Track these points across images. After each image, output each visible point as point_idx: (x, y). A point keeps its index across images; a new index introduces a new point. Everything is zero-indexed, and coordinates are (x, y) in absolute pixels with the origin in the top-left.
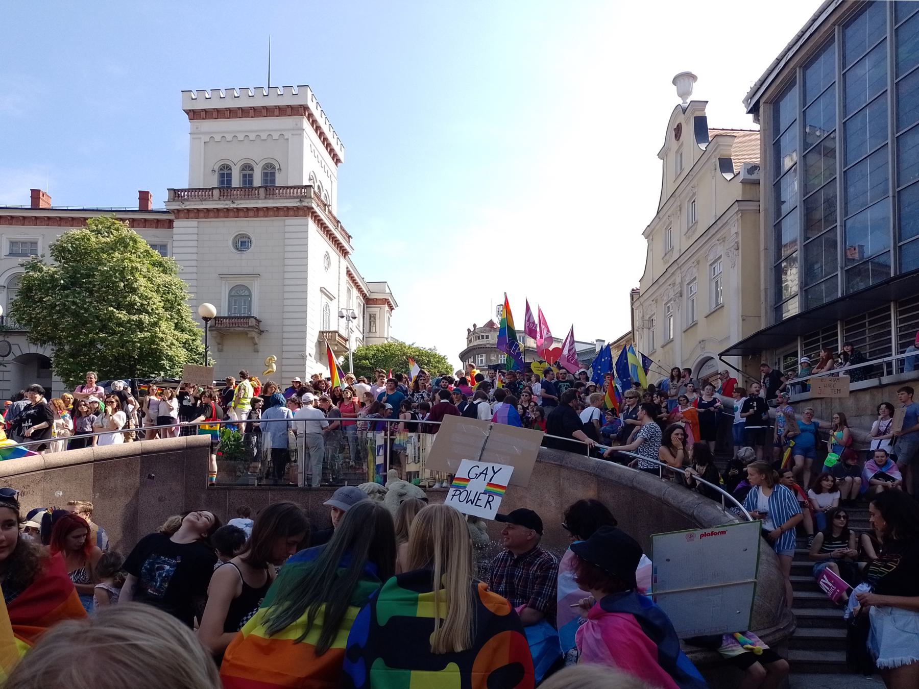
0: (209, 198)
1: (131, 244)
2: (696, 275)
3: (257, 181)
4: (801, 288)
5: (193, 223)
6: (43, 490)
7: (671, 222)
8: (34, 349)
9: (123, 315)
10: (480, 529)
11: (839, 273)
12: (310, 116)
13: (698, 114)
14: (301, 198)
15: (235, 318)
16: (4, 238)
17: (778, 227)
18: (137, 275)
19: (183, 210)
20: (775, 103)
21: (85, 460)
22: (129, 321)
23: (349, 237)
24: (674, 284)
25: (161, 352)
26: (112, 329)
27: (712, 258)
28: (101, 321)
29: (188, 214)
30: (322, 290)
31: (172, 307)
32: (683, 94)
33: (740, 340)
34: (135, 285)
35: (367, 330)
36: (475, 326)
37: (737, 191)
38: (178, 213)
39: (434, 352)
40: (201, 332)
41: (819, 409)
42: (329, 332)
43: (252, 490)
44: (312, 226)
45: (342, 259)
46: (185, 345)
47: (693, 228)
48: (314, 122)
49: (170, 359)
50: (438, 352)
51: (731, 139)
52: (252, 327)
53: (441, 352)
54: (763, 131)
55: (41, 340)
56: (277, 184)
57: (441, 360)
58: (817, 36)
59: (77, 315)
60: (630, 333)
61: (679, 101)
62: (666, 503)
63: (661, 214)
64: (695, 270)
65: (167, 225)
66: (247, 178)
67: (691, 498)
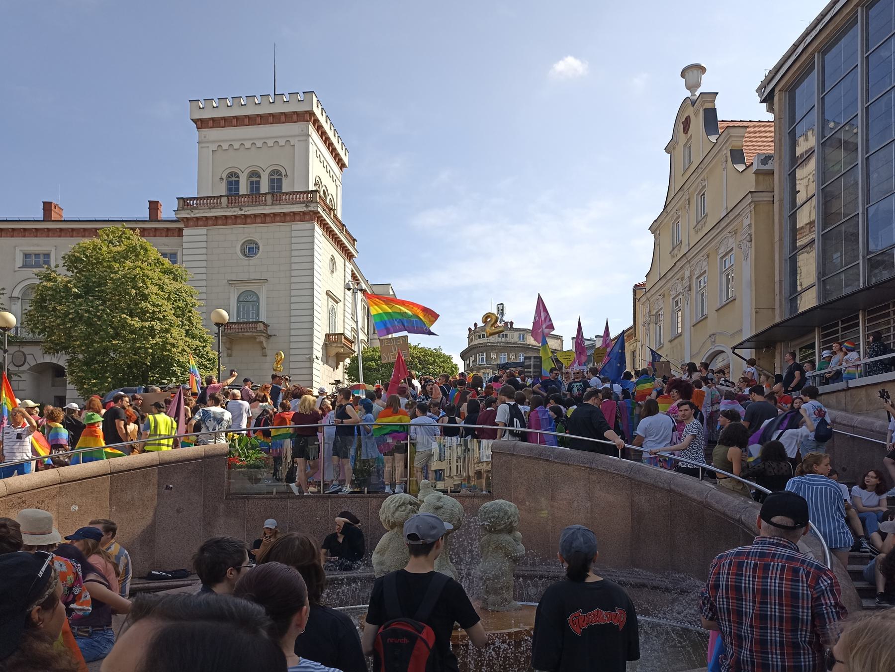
0: (219, 206)
1: (142, 252)
2: (706, 268)
3: (264, 188)
4: (819, 279)
5: (202, 231)
6: (58, 505)
7: (679, 216)
8: (48, 359)
9: (136, 323)
10: (515, 540)
11: (861, 262)
12: (316, 121)
13: (708, 106)
14: (307, 203)
15: (244, 323)
16: (17, 249)
17: (793, 217)
18: (149, 282)
19: (192, 218)
20: (791, 90)
21: (101, 473)
22: (142, 328)
23: (354, 240)
24: (682, 279)
25: (173, 358)
26: (124, 337)
27: (722, 251)
28: (113, 328)
29: (197, 222)
30: (328, 293)
31: (183, 314)
32: (691, 87)
33: (754, 334)
34: (146, 292)
35: (371, 332)
36: (476, 325)
37: (750, 182)
38: (187, 221)
39: (439, 352)
40: (211, 338)
41: (843, 401)
42: (335, 334)
43: (271, 498)
44: (318, 231)
45: (347, 263)
46: (196, 352)
47: (703, 222)
48: (319, 128)
49: (181, 365)
50: (443, 352)
51: (743, 130)
52: (261, 331)
53: (446, 352)
54: (778, 121)
55: (54, 348)
56: (285, 189)
57: (447, 359)
58: (838, 19)
59: (91, 324)
60: (631, 328)
61: (688, 94)
62: (708, 506)
63: (669, 209)
64: (705, 264)
65: (164, 234)
66: (255, 186)
67: (737, 502)
